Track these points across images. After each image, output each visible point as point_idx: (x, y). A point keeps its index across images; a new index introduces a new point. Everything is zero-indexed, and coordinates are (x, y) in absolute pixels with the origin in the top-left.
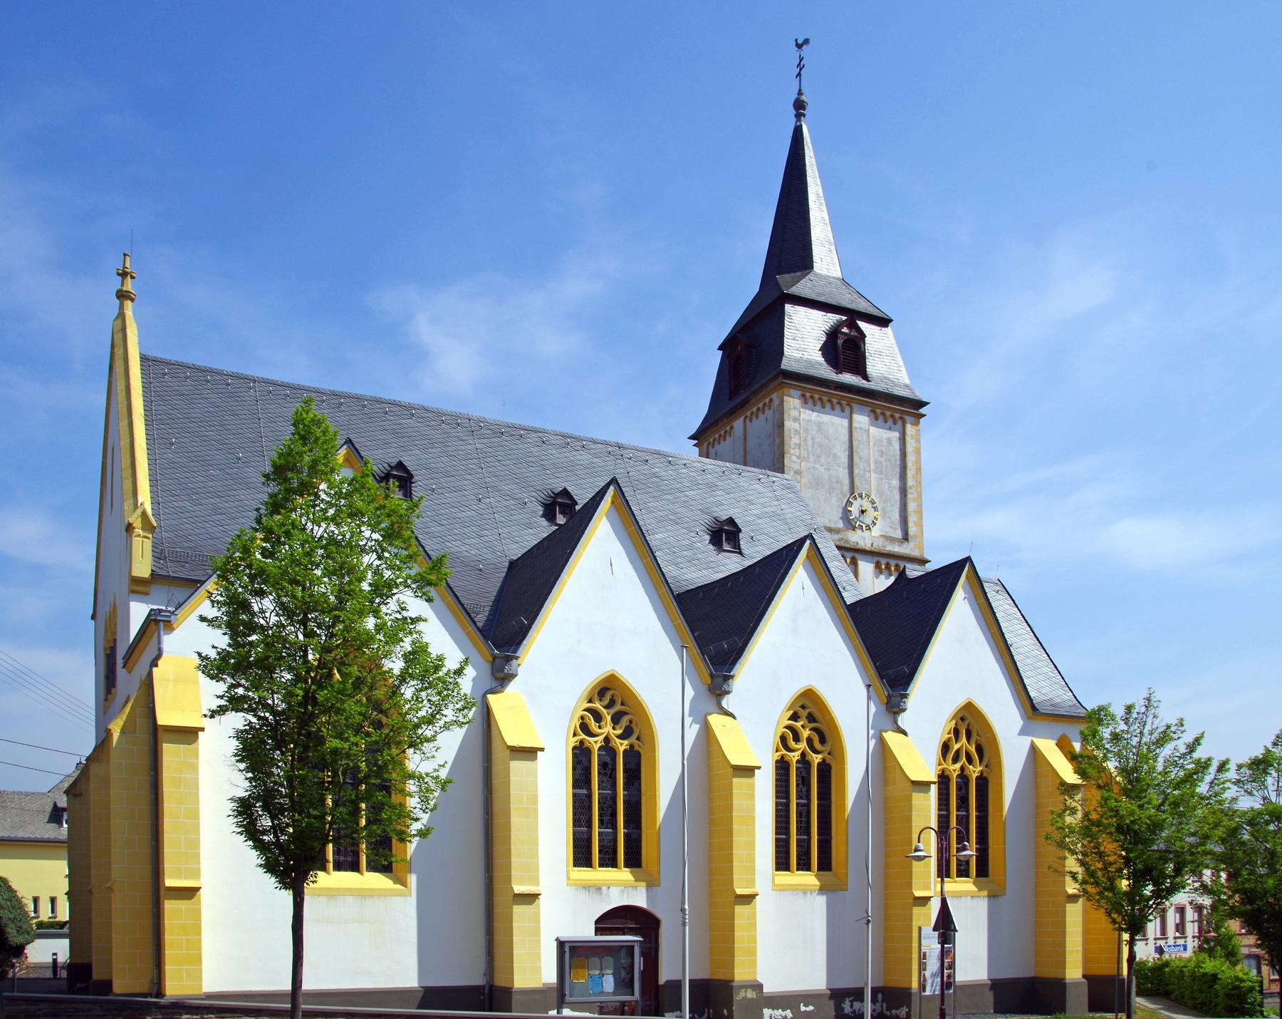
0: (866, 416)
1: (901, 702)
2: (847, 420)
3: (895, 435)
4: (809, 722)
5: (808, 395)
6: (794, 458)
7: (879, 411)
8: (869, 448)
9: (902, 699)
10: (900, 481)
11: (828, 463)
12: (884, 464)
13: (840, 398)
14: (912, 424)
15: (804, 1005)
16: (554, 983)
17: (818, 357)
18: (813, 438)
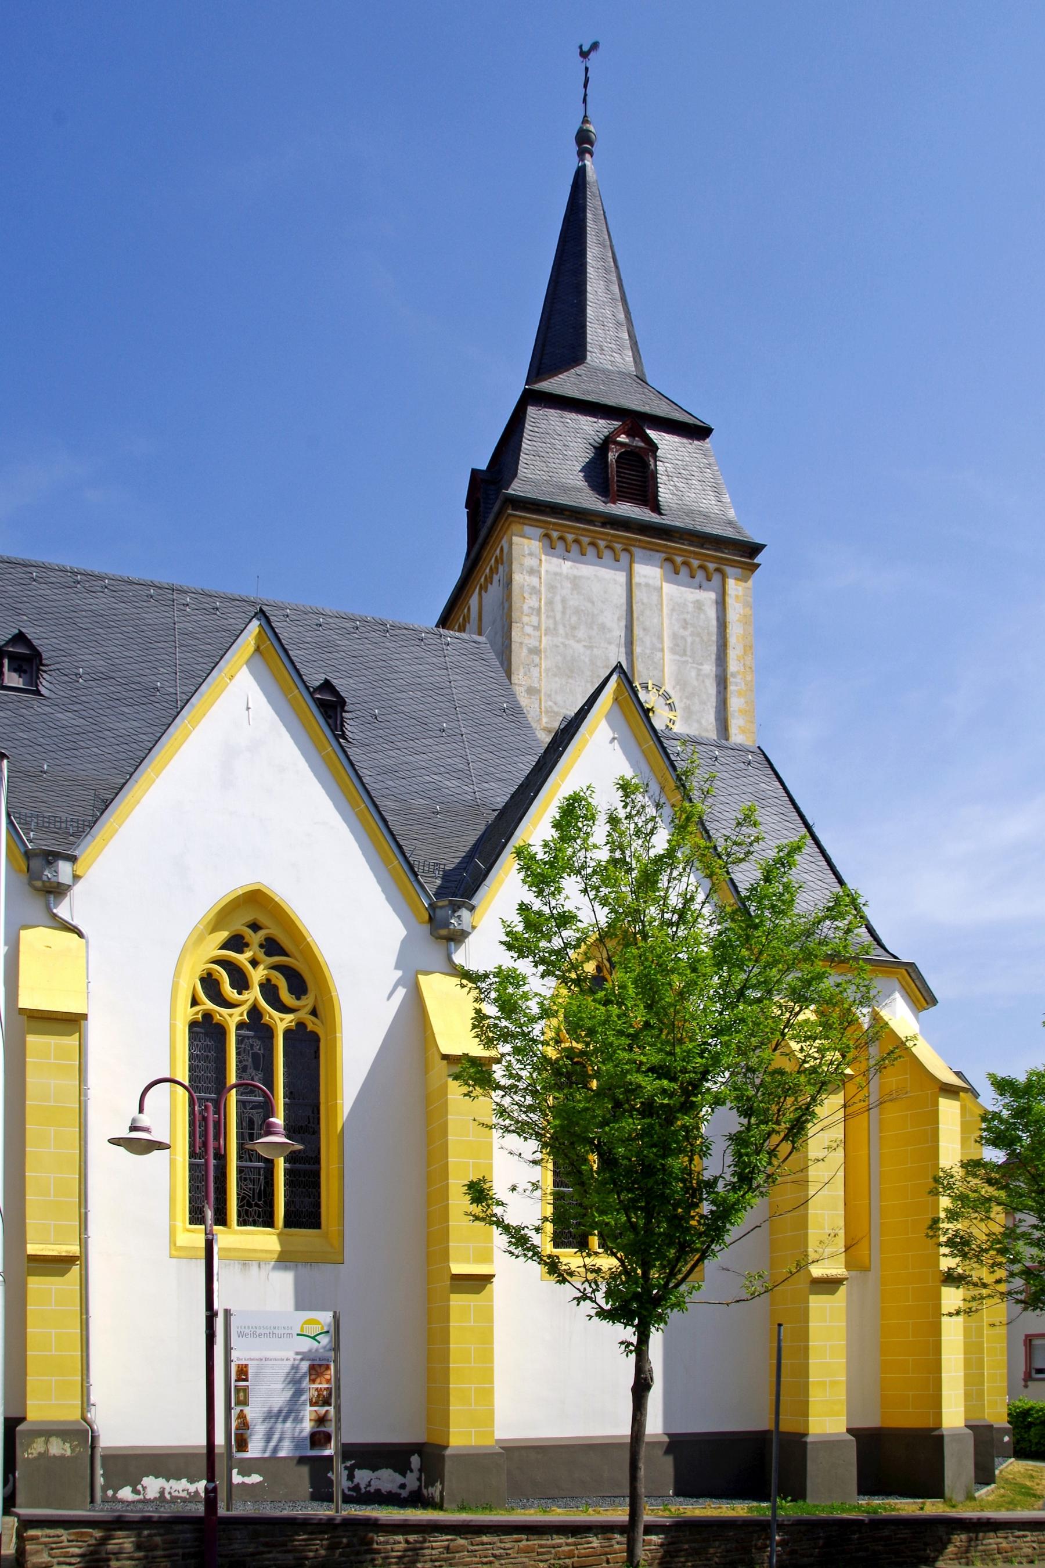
0: (656, 566)
1: (453, 916)
2: (624, 574)
3: (709, 597)
4: (268, 954)
5: (555, 535)
6: (529, 630)
7: (679, 560)
8: (661, 615)
9: (454, 911)
10: (717, 665)
11: (590, 638)
12: (689, 640)
13: (610, 538)
14: (736, 579)
15: (238, 1473)
16: (202, 1447)
17: (578, 480)
18: (564, 601)
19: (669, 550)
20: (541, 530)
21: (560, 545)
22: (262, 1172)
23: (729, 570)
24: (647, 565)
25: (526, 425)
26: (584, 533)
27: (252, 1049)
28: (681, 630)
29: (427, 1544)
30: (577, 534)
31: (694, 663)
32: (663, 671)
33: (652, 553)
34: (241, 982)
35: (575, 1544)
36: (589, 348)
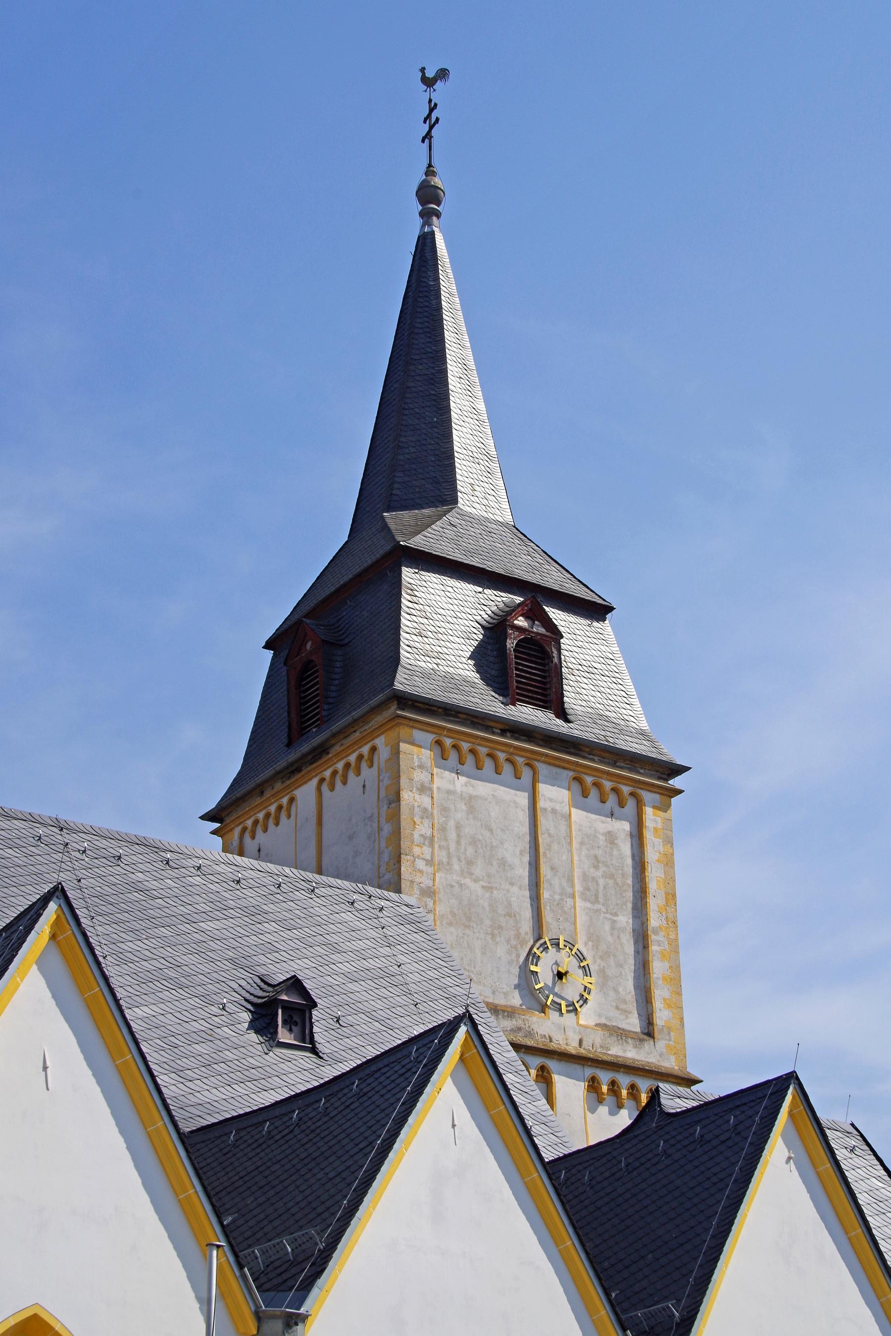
5: (448, 742)
6: (421, 864)
7: (589, 780)
10: (634, 917)
11: (489, 876)
12: (601, 882)
14: (654, 807)
17: (468, 671)
18: (458, 827)
23: (647, 796)
28: (592, 870)
32: (575, 923)
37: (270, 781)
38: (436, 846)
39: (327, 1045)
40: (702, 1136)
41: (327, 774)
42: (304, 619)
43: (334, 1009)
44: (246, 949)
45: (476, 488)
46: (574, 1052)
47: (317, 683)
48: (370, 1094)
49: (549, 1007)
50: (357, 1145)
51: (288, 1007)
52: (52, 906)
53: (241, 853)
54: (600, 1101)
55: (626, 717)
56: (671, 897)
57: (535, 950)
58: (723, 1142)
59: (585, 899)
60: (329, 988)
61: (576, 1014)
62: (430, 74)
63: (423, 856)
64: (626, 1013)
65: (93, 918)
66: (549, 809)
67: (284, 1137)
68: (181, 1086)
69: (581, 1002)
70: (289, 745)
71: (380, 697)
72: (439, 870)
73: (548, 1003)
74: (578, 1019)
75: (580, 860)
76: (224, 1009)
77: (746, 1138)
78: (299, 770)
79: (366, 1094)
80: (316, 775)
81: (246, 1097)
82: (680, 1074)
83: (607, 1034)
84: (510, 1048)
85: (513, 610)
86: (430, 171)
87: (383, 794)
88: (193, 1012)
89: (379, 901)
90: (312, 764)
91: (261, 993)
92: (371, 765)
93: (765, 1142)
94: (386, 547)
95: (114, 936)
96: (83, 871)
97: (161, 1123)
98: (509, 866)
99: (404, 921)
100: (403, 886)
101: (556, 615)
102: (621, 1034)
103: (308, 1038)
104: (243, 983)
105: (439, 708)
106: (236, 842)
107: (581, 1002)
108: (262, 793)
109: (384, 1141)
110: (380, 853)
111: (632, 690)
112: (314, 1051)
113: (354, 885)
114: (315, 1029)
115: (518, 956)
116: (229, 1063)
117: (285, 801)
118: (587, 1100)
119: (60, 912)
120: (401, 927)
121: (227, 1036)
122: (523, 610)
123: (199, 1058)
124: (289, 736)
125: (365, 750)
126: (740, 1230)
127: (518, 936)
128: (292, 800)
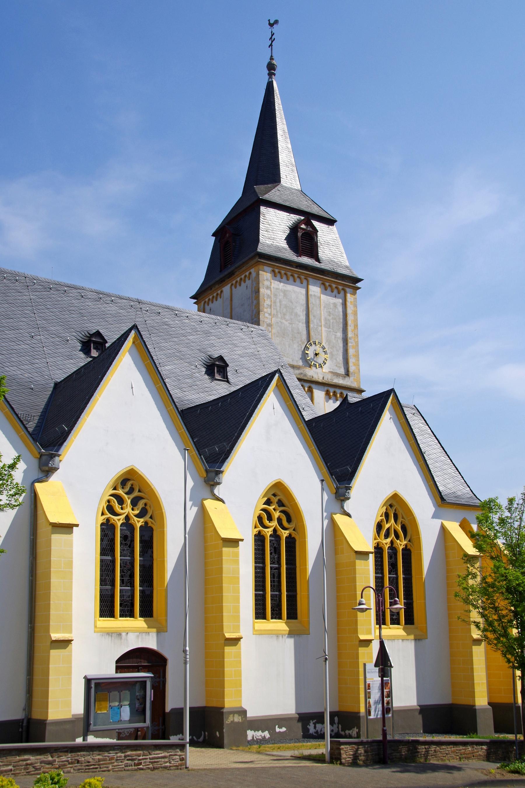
2: (305, 290)
5: (277, 271)
6: (267, 315)
7: (327, 284)
10: (343, 333)
11: (291, 319)
12: (331, 321)
14: (351, 294)
17: (284, 244)
18: (280, 301)
19: (323, 280)
20: (272, 268)
21: (278, 276)
22: (278, 596)
23: (348, 290)
24: (314, 286)
25: (261, 216)
26: (289, 271)
27: (274, 545)
28: (328, 317)
29: (430, 749)
30: (286, 271)
31: (333, 332)
32: (322, 336)
33: (317, 281)
34: (270, 519)
35: (465, 749)
36: (281, 176)
37: (214, 284)
38: (272, 308)
39: (233, 379)
40: (361, 411)
41: (234, 282)
42: (226, 226)
43: (235, 367)
44: (204, 346)
45: (288, 176)
46: (321, 381)
47: (230, 249)
48: (245, 397)
49: (312, 366)
50: (240, 415)
51: (218, 366)
52: (133, 332)
53: (204, 312)
54: (330, 398)
55: (341, 261)
56: (356, 326)
57: (307, 345)
58: (368, 413)
59: (325, 327)
60: (233, 360)
61: (322, 368)
62: (272, 22)
63: (268, 312)
64: (340, 367)
65: (150, 334)
66: (313, 295)
67: (216, 412)
68: (181, 393)
69: (324, 364)
70: (221, 271)
71: (253, 254)
72: (273, 317)
73: (312, 364)
74: (322, 370)
75: (324, 313)
76: (196, 367)
77: (376, 411)
78: (224, 281)
79: (244, 397)
80: (230, 283)
81: (204, 398)
82: (358, 388)
83: (333, 375)
84: (297, 380)
85: (300, 222)
86: (272, 58)
87: (253, 289)
88: (185, 368)
89: (251, 328)
90: (228, 278)
91: (209, 361)
92: (249, 279)
93: (382, 413)
94: (255, 199)
95: (158, 341)
96: (147, 318)
97: (172, 407)
98: (299, 315)
99: (260, 336)
100: (260, 323)
101: (315, 223)
102: (337, 375)
103: (226, 377)
104: (203, 358)
105: (273, 258)
106: (202, 307)
107: (324, 364)
108: (211, 289)
109: (249, 413)
110: (253, 311)
111: (343, 251)
112: (228, 381)
113: (242, 323)
114: (228, 374)
115: (301, 348)
116: (198, 386)
117: (219, 292)
118: (325, 398)
119: (136, 334)
120: (259, 338)
121: (197, 376)
122: (304, 222)
123: (188, 384)
124: (221, 268)
125: (247, 273)
126: (373, 442)
127: (301, 340)
128: (222, 292)
